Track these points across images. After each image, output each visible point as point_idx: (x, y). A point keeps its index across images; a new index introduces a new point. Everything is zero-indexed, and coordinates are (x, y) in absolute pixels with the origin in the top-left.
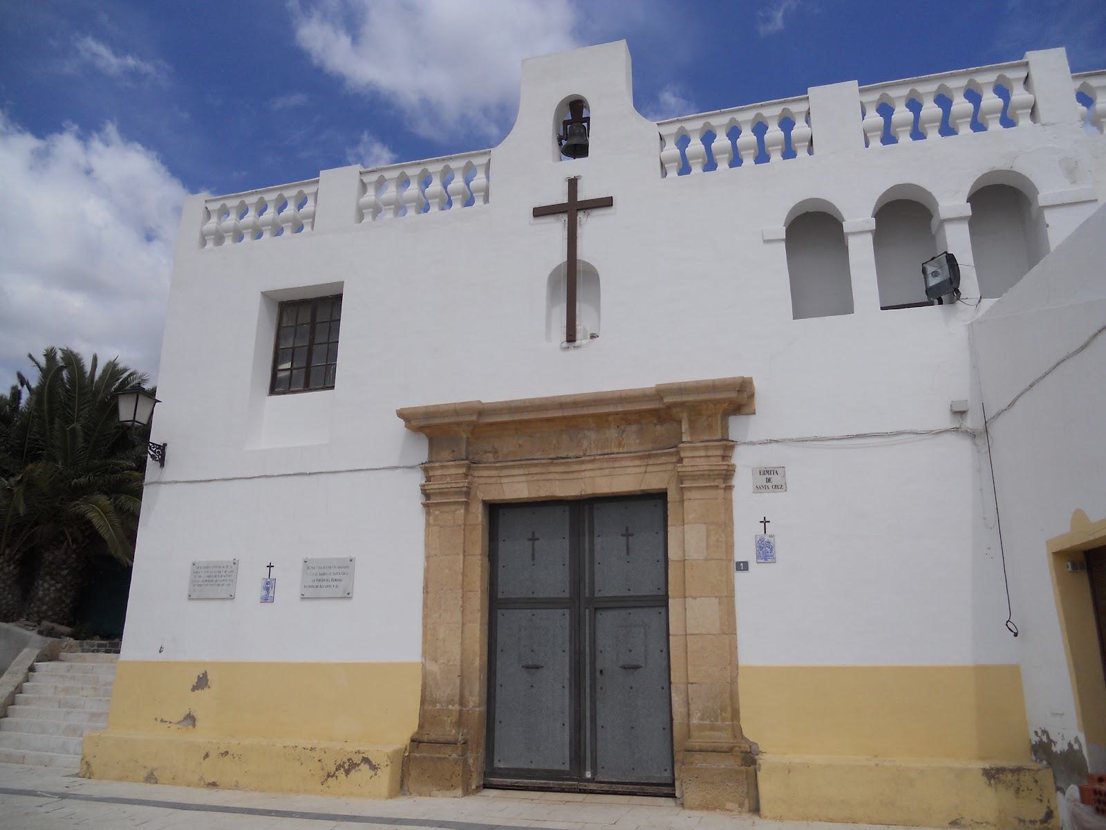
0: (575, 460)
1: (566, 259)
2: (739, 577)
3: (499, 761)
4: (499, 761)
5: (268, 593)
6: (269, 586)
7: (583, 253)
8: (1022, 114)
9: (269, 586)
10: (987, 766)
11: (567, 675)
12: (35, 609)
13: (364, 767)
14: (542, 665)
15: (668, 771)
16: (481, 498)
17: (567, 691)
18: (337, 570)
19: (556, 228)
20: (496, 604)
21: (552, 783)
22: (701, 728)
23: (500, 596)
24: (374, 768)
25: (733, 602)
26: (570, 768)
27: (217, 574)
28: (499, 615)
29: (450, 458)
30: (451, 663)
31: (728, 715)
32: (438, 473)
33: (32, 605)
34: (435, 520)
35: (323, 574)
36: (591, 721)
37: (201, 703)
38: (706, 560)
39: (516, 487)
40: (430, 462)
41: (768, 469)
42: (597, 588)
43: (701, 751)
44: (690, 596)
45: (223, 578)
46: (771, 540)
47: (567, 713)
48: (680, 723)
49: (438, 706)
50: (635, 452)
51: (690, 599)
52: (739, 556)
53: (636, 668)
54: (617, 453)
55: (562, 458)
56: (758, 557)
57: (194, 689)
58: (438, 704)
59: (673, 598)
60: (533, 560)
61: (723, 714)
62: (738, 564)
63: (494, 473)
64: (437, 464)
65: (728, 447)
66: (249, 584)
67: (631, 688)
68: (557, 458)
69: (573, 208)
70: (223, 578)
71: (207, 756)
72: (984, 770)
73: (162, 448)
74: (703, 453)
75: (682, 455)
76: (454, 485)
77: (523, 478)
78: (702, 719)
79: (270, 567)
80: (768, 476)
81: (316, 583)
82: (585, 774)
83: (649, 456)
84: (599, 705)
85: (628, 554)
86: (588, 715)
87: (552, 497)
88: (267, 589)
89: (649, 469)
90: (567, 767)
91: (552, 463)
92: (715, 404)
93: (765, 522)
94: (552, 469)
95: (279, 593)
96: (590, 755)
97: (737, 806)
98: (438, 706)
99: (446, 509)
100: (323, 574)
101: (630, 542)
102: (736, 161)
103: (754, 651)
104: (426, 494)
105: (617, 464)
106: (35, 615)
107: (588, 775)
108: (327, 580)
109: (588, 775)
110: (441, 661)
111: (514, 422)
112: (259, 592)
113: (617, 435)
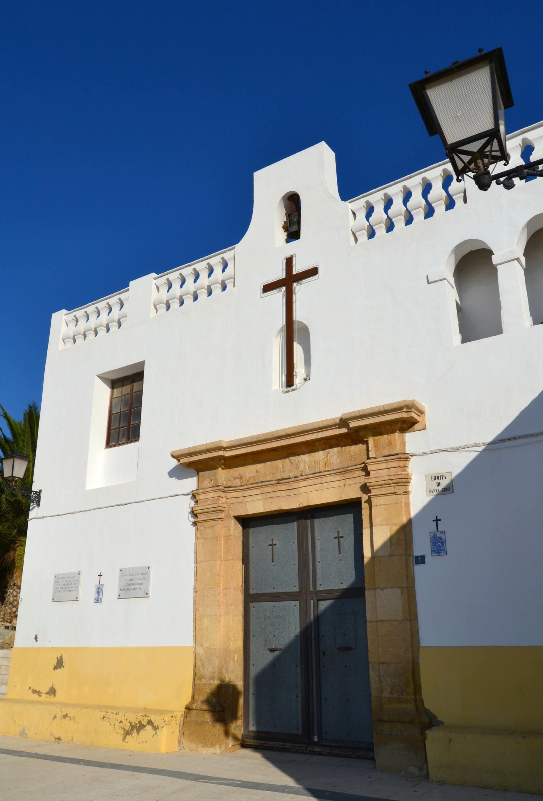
1: (285, 323)
2: (418, 569)
5: (99, 596)
6: (99, 590)
7: (297, 316)
8: (437, 205)
9: (99, 590)
12: (8, 611)
13: (149, 728)
17: (299, 669)
19: (278, 296)
20: (250, 598)
21: (288, 745)
27: (69, 583)
28: (251, 608)
29: (210, 486)
30: (212, 647)
33: (6, 608)
34: (201, 534)
35: (132, 580)
37: (58, 678)
38: (390, 556)
39: (256, 505)
40: (198, 489)
41: (438, 475)
44: (379, 588)
45: (72, 586)
46: (443, 535)
49: (204, 681)
50: (337, 469)
52: (417, 552)
53: (349, 649)
55: (287, 479)
56: (433, 551)
57: (55, 668)
58: (203, 680)
59: (369, 589)
61: (408, 689)
62: (417, 558)
63: (240, 494)
64: (201, 491)
65: (404, 458)
66: (86, 590)
67: (346, 666)
68: (283, 479)
69: (289, 280)
70: (72, 586)
71: (55, 717)
73: (39, 494)
74: (384, 466)
75: (369, 468)
77: (259, 497)
78: (391, 693)
79: (100, 576)
80: (438, 481)
83: (346, 472)
87: (279, 510)
89: (348, 482)
90: (300, 732)
91: (278, 483)
92: (390, 425)
93: (437, 520)
94: (279, 487)
97: (418, 769)
98: (204, 681)
100: (132, 580)
101: (341, 543)
102: (429, 212)
103: (435, 631)
104: (194, 514)
105: (324, 480)
106: (9, 615)
107: (316, 740)
108: (134, 584)
110: (205, 645)
112: (93, 595)
113: (323, 457)
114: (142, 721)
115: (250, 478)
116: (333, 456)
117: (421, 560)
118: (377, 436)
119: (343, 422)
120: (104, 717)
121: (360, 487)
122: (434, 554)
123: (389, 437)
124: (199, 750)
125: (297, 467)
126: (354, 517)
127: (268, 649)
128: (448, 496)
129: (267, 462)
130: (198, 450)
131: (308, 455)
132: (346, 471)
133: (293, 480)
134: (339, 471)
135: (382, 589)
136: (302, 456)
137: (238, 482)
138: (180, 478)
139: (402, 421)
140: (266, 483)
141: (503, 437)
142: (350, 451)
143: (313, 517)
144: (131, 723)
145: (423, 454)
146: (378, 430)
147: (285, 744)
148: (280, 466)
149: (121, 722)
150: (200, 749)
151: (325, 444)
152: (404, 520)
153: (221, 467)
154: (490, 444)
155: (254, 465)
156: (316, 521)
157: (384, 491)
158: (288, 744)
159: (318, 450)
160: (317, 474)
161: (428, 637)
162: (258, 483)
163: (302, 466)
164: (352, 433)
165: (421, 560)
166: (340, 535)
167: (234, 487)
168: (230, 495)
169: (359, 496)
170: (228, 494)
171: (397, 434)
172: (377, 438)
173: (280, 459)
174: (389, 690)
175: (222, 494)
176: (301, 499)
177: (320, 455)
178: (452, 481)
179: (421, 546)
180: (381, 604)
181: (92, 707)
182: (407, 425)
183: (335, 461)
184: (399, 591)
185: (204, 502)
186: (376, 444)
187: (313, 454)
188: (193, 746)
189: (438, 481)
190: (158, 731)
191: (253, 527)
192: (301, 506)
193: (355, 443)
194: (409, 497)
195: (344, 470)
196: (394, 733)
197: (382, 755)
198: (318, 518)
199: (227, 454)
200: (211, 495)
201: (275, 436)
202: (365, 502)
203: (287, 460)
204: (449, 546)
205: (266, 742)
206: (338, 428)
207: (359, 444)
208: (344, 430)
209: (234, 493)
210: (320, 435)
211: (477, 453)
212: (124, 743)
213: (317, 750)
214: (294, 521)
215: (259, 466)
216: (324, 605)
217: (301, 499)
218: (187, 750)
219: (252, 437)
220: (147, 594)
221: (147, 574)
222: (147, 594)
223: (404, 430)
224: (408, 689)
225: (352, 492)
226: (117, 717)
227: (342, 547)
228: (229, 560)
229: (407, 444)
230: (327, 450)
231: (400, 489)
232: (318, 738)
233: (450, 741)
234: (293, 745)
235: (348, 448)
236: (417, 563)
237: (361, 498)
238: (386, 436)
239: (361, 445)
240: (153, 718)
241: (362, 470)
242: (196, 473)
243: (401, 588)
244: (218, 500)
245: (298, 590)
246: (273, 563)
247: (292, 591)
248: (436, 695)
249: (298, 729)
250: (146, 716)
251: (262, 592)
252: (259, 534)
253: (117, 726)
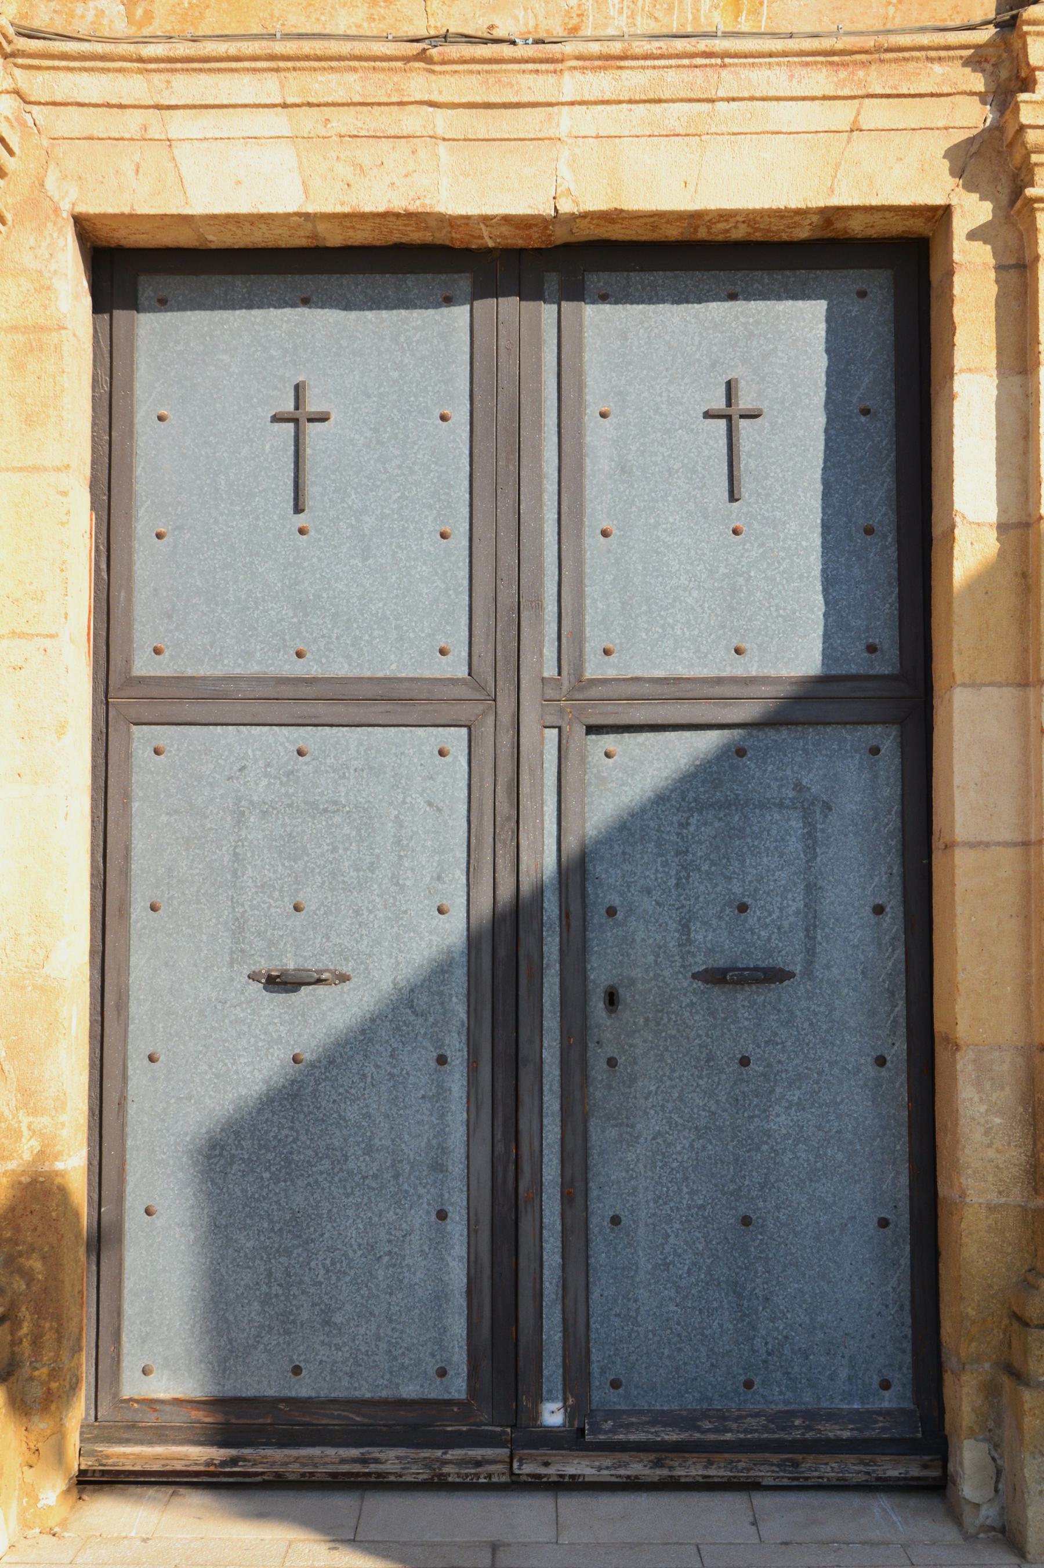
3: (146, 1371)
4: (146, 1371)
11: (460, 1010)
14: (346, 969)
15: (896, 1387)
16: (66, 207)
20: (123, 699)
21: (391, 1460)
23: (144, 665)
26: (471, 1390)
36: (567, 1197)
47: (457, 1167)
48: (992, 1209)
54: (727, 35)
59: (974, 685)
63: (132, 87)
67: (745, 1062)
77: (278, 123)
82: (536, 1415)
86: (551, 1172)
89: (875, 114)
90: (457, 1387)
91: (422, 57)
94: (418, 84)
96: (558, 1337)
105: (729, 81)
109: (553, 1415)
121: (949, 154)
126: (830, 318)
127: (253, 977)
132: (878, 49)
147: (375, 1452)
156: (596, 317)
158: (391, 1453)
169: (939, 200)
170: (40, 77)
195: (869, 42)
202: (972, 236)
205: (246, 1451)
209: (84, 79)
217: (564, 170)
228: (36, 469)
232: (571, 1413)
234: (425, 1453)
241: (967, 62)
246: (301, 520)
247: (427, 674)
251: (219, 671)
252: (211, 357)
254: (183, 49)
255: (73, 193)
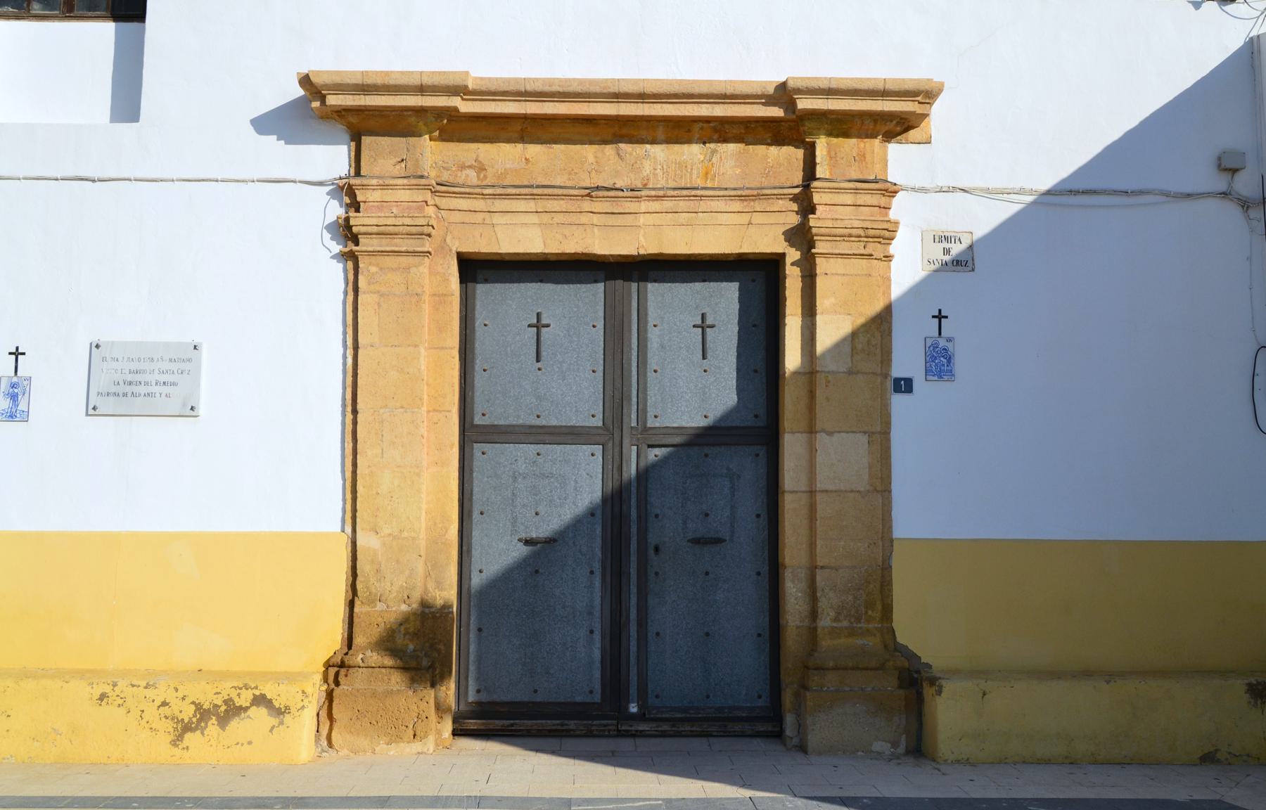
0: (630, 194)
10: (1253, 681)
13: (259, 713)
16: (454, 250)
17: (598, 583)
18: (166, 366)
20: (472, 433)
21: (572, 724)
22: (834, 633)
23: (478, 420)
24: (280, 712)
25: (889, 440)
28: (477, 454)
29: (396, 173)
30: (405, 534)
31: (876, 613)
32: (375, 196)
42: (650, 414)
43: (836, 668)
44: (823, 431)
46: (950, 345)
47: (597, 614)
48: (798, 627)
49: (380, 606)
51: (824, 435)
52: (898, 371)
60: (538, 361)
61: (870, 612)
62: (897, 381)
63: (479, 204)
64: (374, 182)
67: (707, 573)
68: (598, 188)
72: (1249, 685)
74: (848, 199)
76: (408, 221)
77: (534, 219)
78: (836, 620)
80: (947, 246)
81: (122, 389)
82: (627, 708)
84: (652, 601)
85: (704, 357)
88: (14, 397)
89: (757, 218)
90: (597, 698)
91: (589, 195)
92: (875, 121)
94: (587, 205)
95: (38, 402)
99: (390, 261)
101: (709, 338)
105: (704, 205)
107: (633, 708)
108: (146, 384)
111: (525, 117)
114: (236, 700)
115: (506, 172)
116: (729, 159)
117: (905, 386)
118: (837, 136)
119: (784, 94)
120: (103, 697)
122: (929, 378)
123: (862, 145)
124: (377, 749)
125: (635, 168)
126: (740, 290)
127: (520, 540)
128: (962, 277)
129: (555, 143)
130: (392, 82)
131: (663, 146)
133: (626, 194)
134: (739, 193)
135: (830, 434)
136: (648, 146)
137: (471, 176)
138: (290, 138)
139: (891, 117)
140: (546, 191)
141: (1075, 186)
142: (766, 157)
143: (644, 278)
144: (198, 706)
145: (923, 190)
146: (842, 125)
148: (591, 159)
149: (164, 704)
150: (381, 747)
151: (715, 130)
152: (878, 306)
153: (430, 133)
154: (1048, 193)
155: (520, 146)
156: (652, 287)
157: (844, 248)
159: (689, 141)
160: (689, 192)
161: (909, 522)
162: (531, 187)
163: (647, 168)
164: (790, 120)
165: (905, 386)
166: (709, 322)
167: (463, 186)
168: (443, 202)
170: (444, 200)
171: (877, 142)
172: (834, 140)
173: (591, 143)
174: (832, 614)
175: (428, 196)
176: (641, 238)
177: (693, 152)
178: (971, 247)
179: (907, 359)
180: (815, 462)
181: (65, 675)
182: (898, 126)
183: (730, 172)
184: (864, 439)
185: (380, 209)
186: (833, 154)
187: (676, 147)
188: (363, 742)
189: (947, 246)
190: (287, 718)
191: (486, 281)
192: (642, 252)
193: (778, 141)
194: (889, 268)
195: (755, 192)
196: (847, 689)
197: (821, 729)
198: (655, 281)
199: (466, 107)
200: (404, 195)
201: (612, 90)
203: (609, 150)
204: (960, 364)
206: (763, 104)
207: (789, 144)
208: (776, 112)
210: (719, 111)
211: (1020, 207)
212: (177, 752)
213: (640, 728)
214: (596, 281)
215: (534, 150)
216: (654, 455)
217: (641, 238)
218: (345, 752)
219: (551, 81)
220: (192, 409)
221: (189, 360)
222: (192, 409)
223: (889, 136)
224: (870, 612)
225: (764, 235)
226: (150, 693)
227: (709, 345)
228: (442, 348)
229: (889, 164)
230: (712, 145)
231: (877, 250)
232: (640, 707)
233: (984, 694)
235: (761, 149)
236: (897, 389)
237: (783, 255)
238: (853, 141)
239: (791, 149)
240: (269, 691)
242: (347, 137)
243: (871, 434)
244: (421, 209)
245: (649, 425)
246: (539, 365)
248: (920, 625)
249: (591, 692)
250: (246, 687)
251: (507, 423)
252: (508, 304)
253: (151, 712)
254: (499, 191)
255: (457, 244)
